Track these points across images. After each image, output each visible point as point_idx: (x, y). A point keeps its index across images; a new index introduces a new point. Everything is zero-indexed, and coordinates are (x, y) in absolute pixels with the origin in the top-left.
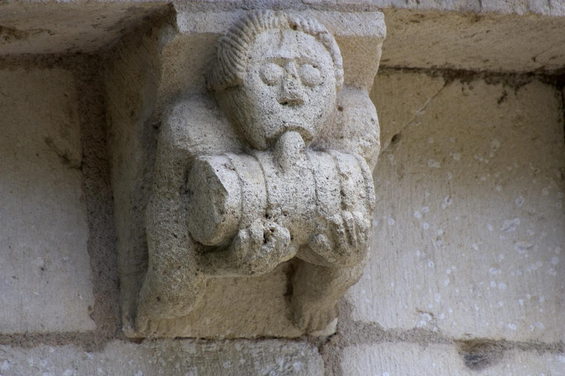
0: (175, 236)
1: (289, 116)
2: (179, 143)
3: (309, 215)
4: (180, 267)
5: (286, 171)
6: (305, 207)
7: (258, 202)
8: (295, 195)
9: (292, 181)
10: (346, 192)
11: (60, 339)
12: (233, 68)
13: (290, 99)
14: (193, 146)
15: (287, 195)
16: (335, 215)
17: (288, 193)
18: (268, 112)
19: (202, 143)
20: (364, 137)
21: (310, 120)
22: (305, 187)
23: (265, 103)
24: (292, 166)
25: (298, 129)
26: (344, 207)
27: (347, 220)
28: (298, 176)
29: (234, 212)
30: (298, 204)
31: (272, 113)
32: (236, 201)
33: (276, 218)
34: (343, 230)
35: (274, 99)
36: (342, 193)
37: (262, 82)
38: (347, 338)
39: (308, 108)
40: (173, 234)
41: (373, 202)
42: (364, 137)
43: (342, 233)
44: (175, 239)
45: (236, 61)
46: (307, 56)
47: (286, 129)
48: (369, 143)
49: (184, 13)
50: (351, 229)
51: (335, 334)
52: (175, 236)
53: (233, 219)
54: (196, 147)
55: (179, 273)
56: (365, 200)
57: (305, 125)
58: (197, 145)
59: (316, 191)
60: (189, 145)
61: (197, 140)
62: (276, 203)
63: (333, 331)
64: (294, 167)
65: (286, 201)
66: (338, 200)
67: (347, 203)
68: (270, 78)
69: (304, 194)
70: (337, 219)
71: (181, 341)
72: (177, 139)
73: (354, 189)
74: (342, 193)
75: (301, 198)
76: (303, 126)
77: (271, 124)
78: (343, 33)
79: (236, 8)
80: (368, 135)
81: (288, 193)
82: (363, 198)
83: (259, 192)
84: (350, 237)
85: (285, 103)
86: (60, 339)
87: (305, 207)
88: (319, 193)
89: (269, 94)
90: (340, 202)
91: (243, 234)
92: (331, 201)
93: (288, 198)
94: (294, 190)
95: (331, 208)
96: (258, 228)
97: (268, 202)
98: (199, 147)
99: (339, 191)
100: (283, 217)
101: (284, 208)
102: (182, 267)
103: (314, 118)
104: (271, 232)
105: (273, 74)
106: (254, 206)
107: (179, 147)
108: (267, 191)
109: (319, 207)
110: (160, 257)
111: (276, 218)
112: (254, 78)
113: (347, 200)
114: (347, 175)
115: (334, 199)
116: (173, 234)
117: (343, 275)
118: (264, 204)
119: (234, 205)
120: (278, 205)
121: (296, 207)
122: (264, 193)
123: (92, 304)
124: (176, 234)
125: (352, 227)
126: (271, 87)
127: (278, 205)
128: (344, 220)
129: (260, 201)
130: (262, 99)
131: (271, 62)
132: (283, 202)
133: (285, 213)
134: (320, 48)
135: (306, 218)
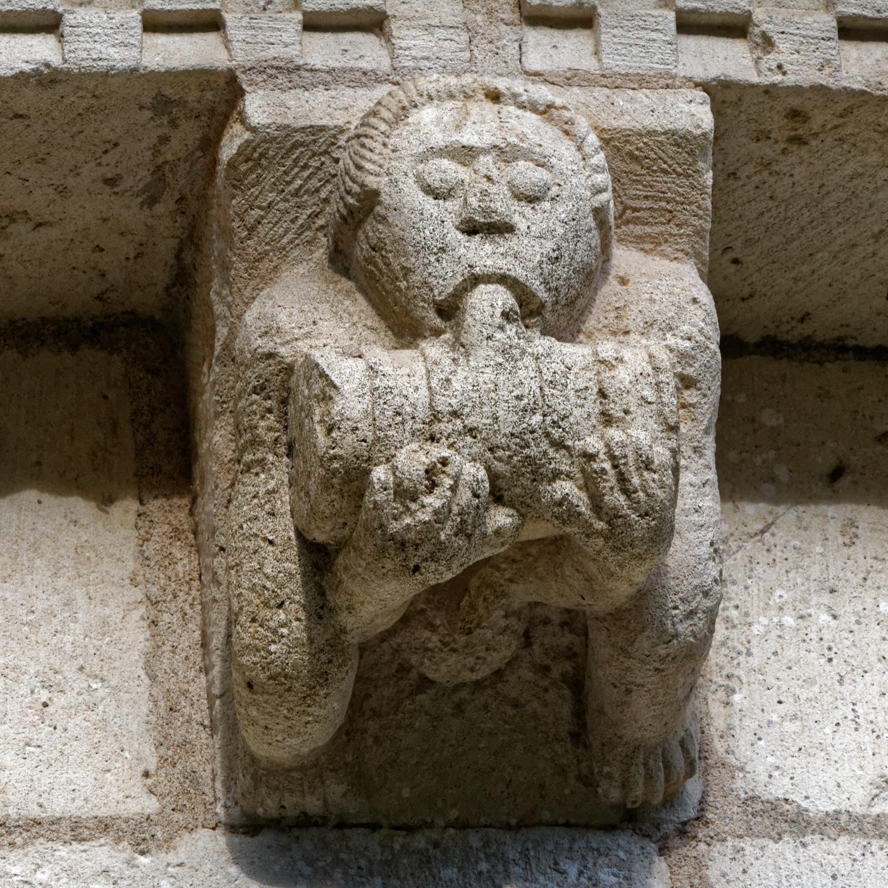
0: (271, 542)
1: (484, 254)
2: (259, 342)
3: (528, 437)
4: (283, 603)
5: (472, 352)
6: (515, 418)
7: (409, 409)
8: (493, 395)
9: (487, 370)
10: (610, 392)
11: (77, 830)
12: (359, 173)
13: (482, 220)
14: (288, 342)
15: (475, 395)
16: (588, 439)
17: (478, 390)
18: (435, 250)
19: (308, 335)
20: (676, 332)
21: (531, 265)
22: (517, 381)
23: (427, 232)
24: (485, 342)
25: (503, 279)
26: (607, 420)
27: (612, 444)
28: (500, 360)
29: (357, 428)
30: (501, 413)
31: (445, 251)
32: (359, 407)
33: (451, 440)
34: (607, 466)
35: (615, 490)
36: (602, 394)
37: (421, 194)
38: (719, 825)
39: (526, 242)
40: (265, 539)
41: (671, 411)
42: (676, 332)
43: (603, 470)
44: (270, 548)
45: (363, 157)
46: (521, 144)
47: (475, 280)
48: (687, 344)
49: (260, 92)
50: (623, 461)
51: (697, 819)
52: (271, 542)
53: (356, 444)
54: (294, 343)
55: (283, 616)
56: (654, 407)
57: (518, 272)
58: (296, 339)
59: (541, 388)
60: (278, 341)
61: (296, 331)
62: (450, 409)
63: (693, 814)
64: (491, 343)
65: (473, 407)
66: (593, 406)
67: (612, 412)
68: (437, 184)
69: (514, 394)
70: (593, 443)
71: (347, 832)
72: (256, 335)
73: (629, 386)
74: (602, 394)
75: (507, 402)
76: (513, 273)
77: (445, 277)
78: (615, 124)
79: (376, 80)
80: (686, 328)
81: (478, 390)
82: (650, 403)
83: (411, 390)
84: (622, 479)
85: (471, 229)
86: (77, 830)
87: (515, 418)
88: (547, 390)
89: (435, 214)
90: (597, 410)
91: (380, 473)
92: (582, 413)
93: (478, 400)
94: (492, 386)
95: (578, 424)
96: (412, 459)
97: (432, 407)
98: (300, 343)
99: (596, 390)
100: (469, 439)
101: (471, 421)
102: (287, 603)
103: (541, 263)
104: (439, 466)
105: (443, 176)
106: (399, 414)
107: (260, 350)
108: (430, 388)
109: (548, 419)
110: (244, 591)
111: (451, 440)
112: (401, 185)
113: (612, 405)
114: (614, 362)
115: (582, 406)
116: (265, 539)
117: (656, 623)
118: (422, 413)
119: (355, 414)
120: (455, 414)
121: (496, 419)
122: (424, 392)
123: (152, 764)
124: (271, 538)
125: (625, 457)
126: (441, 202)
127: (455, 414)
128: (607, 445)
129: (413, 405)
130: (420, 225)
131: (441, 157)
132: (467, 410)
133: (471, 431)
134: (550, 134)
135: (522, 443)
